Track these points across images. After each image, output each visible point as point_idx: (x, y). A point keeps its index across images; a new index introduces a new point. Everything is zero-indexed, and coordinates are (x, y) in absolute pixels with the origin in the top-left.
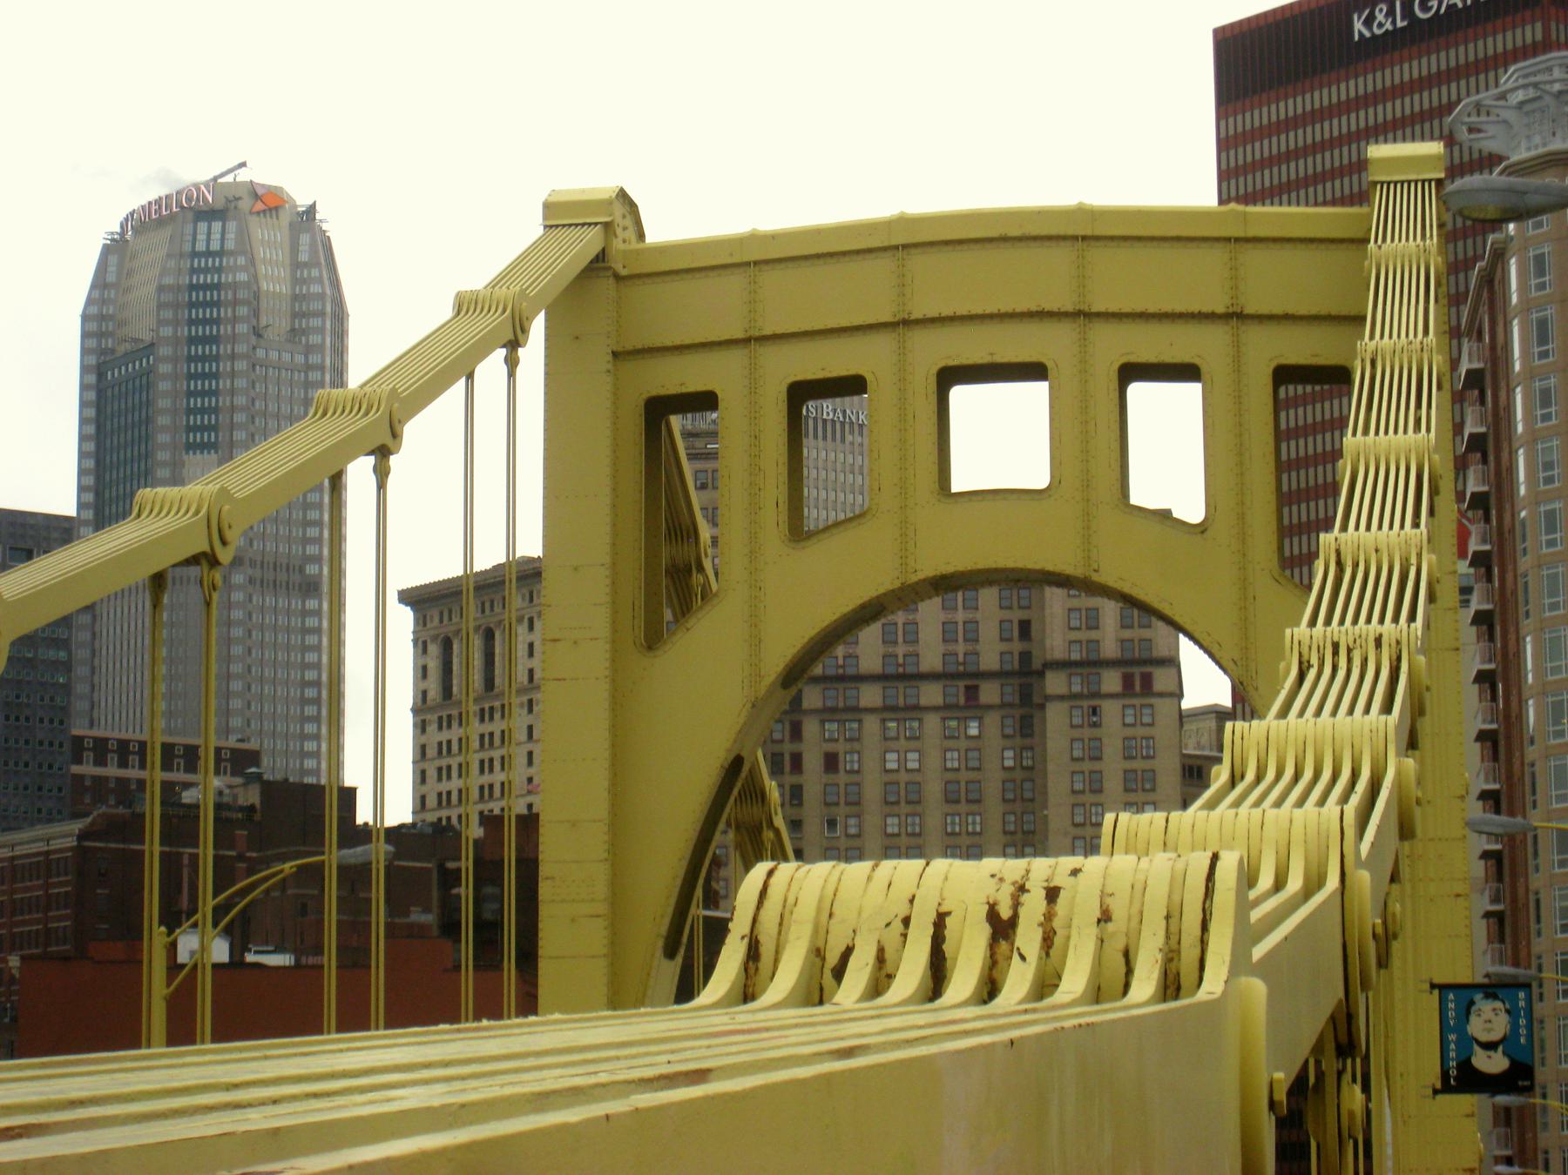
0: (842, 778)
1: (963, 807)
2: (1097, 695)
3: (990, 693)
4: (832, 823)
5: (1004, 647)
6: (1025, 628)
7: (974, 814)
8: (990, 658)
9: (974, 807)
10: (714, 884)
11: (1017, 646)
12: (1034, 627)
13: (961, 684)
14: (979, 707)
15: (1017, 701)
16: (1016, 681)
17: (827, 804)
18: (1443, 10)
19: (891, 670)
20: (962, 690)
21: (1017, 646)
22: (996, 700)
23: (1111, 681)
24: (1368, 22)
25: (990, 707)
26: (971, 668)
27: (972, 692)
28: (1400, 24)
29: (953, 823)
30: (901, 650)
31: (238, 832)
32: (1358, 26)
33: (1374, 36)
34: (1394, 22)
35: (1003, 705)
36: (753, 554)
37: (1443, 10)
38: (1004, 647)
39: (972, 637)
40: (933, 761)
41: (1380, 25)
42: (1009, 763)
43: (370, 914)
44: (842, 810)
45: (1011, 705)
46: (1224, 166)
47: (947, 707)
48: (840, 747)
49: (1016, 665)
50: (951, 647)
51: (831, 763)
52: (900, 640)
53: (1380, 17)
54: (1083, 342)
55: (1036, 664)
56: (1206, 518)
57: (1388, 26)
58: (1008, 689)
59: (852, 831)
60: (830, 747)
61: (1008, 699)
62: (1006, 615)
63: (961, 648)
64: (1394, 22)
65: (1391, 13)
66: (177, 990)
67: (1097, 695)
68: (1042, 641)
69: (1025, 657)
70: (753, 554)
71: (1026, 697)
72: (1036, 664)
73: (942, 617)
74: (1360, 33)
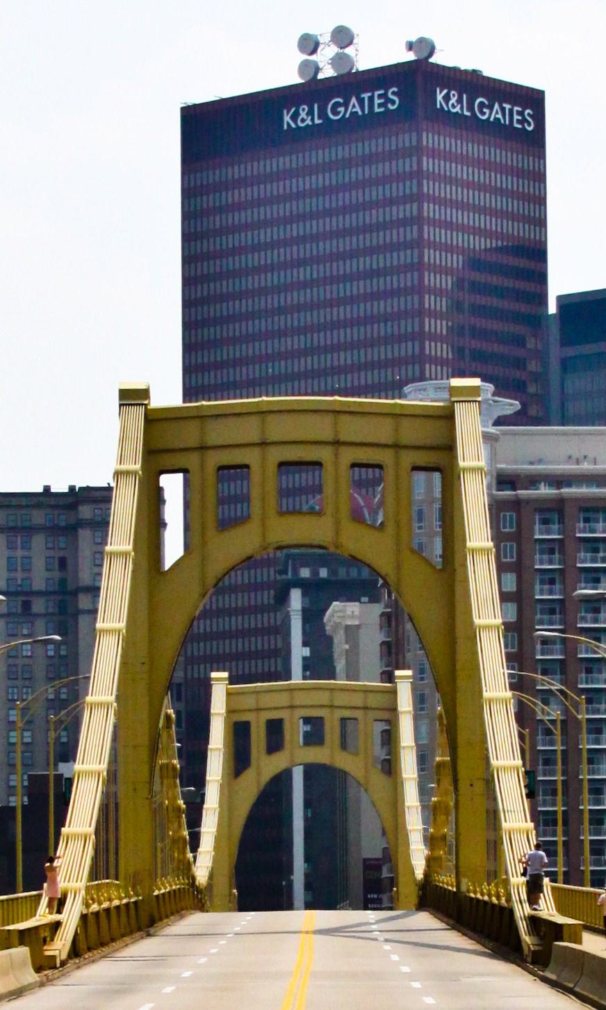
1: (19, 683)
3: (38, 606)
5: (47, 574)
6: (63, 563)
7: (27, 687)
8: (39, 584)
9: (27, 683)
10: (562, 587)
11: (57, 574)
12: (70, 562)
14: (30, 614)
15: (57, 610)
18: (347, 116)
20: (20, 603)
21: (57, 574)
22: (43, 611)
24: (295, 117)
25: (38, 615)
26: (26, 589)
27: (27, 606)
28: (317, 121)
29: (13, 694)
32: (287, 119)
34: (312, 120)
35: (9, 615)
36: (203, 535)
37: (347, 116)
38: (47, 574)
39: (27, 569)
41: (303, 120)
42: (51, 653)
43: (90, 672)
45: (52, 614)
49: (57, 588)
50: (12, 575)
52: (19, 569)
53: (303, 115)
54: (263, 422)
55: (70, 587)
57: (309, 122)
58: (51, 604)
61: (51, 610)
62: (51, 553)
63: (20, 575)
64: (312, 120)
65: (311, 113)
68: (76, 572)
69: (63, 582)
70: (203, 535)
72: (70, 587)
74: (288, 124)
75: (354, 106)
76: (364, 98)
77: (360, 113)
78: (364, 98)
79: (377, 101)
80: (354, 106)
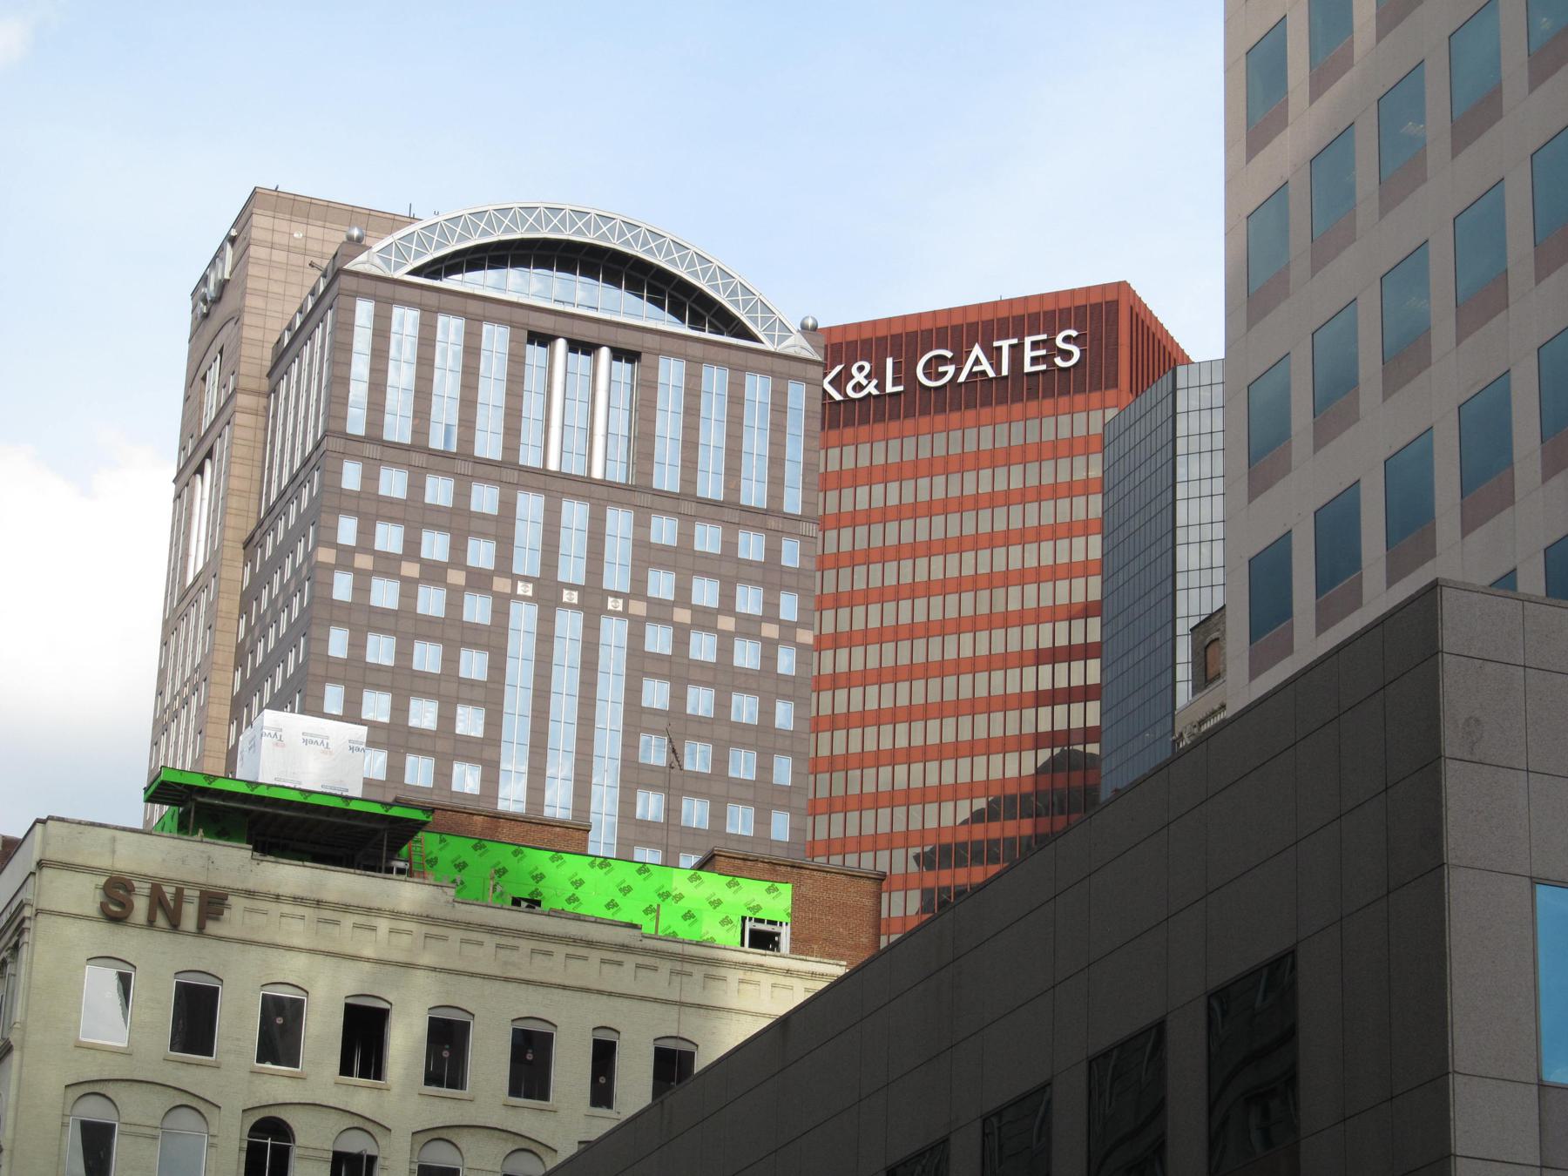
28: (890, 389)
41: (859, 387)
53: (859, 377)
57: (871, 389)
65: (878, 373)
75: (977, 362)
76: (1000, 349)
77: (991, 374)
78: (1000, 349)
79: (1028, 354)
80: (977, 362)
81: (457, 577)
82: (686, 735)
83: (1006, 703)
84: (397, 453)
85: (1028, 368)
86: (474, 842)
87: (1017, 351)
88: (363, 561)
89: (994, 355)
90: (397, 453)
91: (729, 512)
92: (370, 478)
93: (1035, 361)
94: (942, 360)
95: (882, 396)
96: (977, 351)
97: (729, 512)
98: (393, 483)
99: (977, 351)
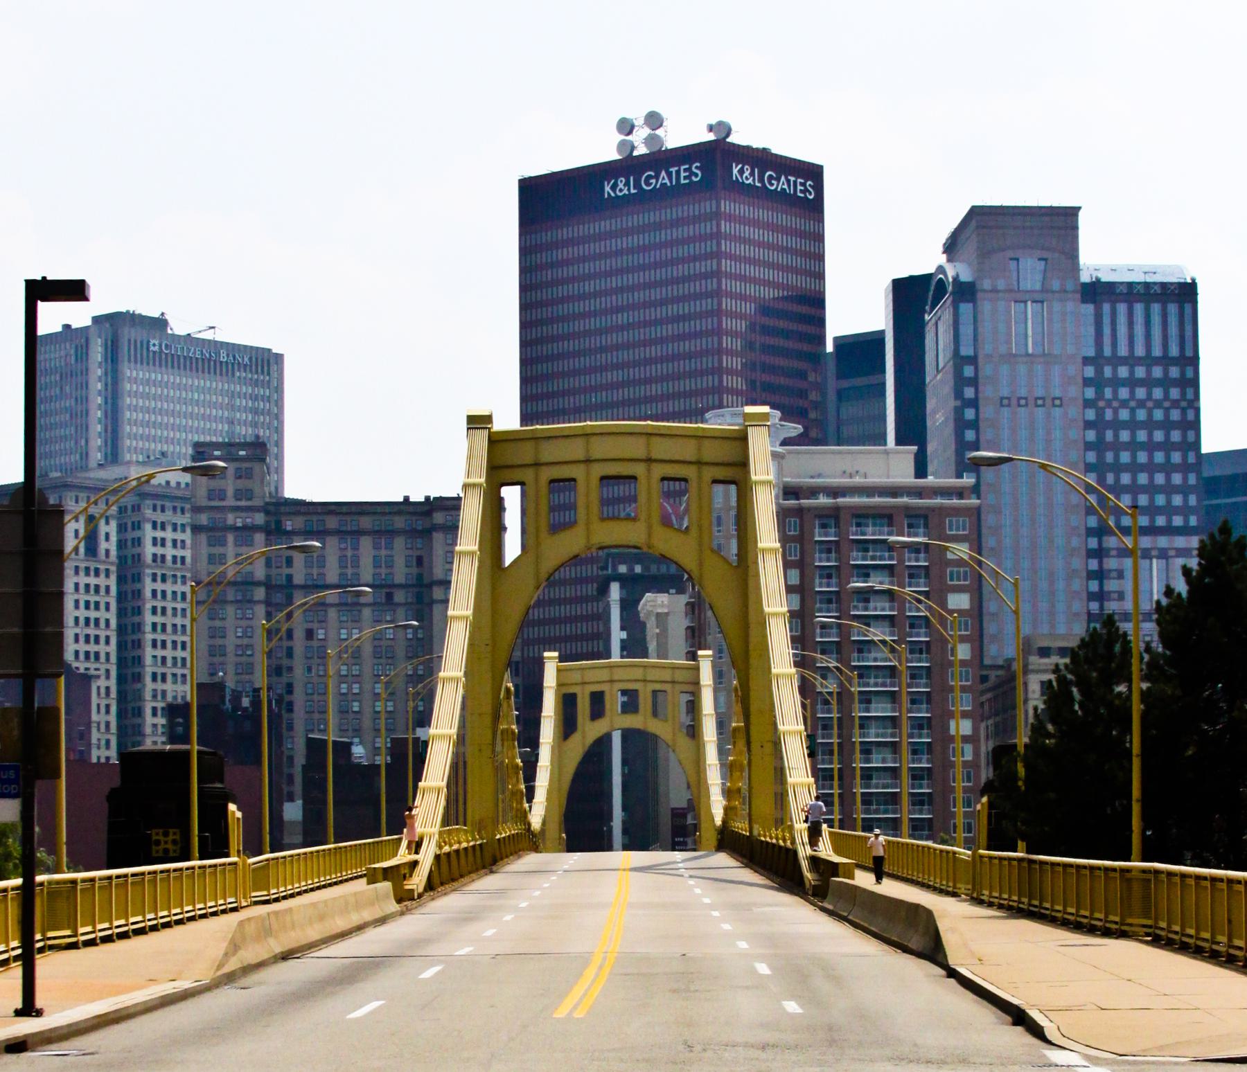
0: (315, 643)
1: (383, 661)
2: (250, 601)
3: (399, 596)
4: (310, 669)
6: (420, 561)
8: (399, 578)
11: (415, 570)
12: (425, 560)
13: (384, 590)
16: (416, 590)
17: (307, 658)
19: (310, 583)
21: (415, 570)
22: (403, 601)
23: (260, 593)
24: (614, 188)
25: (399, 604)
27: (389, 596)
28: (633, 191)
30: (315, 571)
31: (546, 654)
32: (607, 189)
33: (617, 197)
39: (390, 565)
40: (332, 634)
41: (621, 190)
44: (316, 661)
46: (1188, 308)
47: (340, 604)
48: (315, 626)
50: (378, 571)
51: (310, 634)
53: (621, 186)
56: (499, 492)
58: (410, 595)
59: (321, 673)
60: (310, 626)
63: (383, 571)
65: (627, 184)
66: (171, 752)
67: (250, 601)
71: (419, 598)
72: (426, 581)
73: (373, 552)
79: (683, 174)
81: (1115, 404)
82: (1129, 443)
83: (594, 314)
84: (1123, 361)
85: (683, 182)
86: (508, 418)
87: (678, 173)
88: (1115, 404)
89: (669, 175)
90: (1123, 361)
91: (1149, 361)
92: (1115, 371)
93: (685, 178)
94: (649, 177)
95: (630, 194)
96: (663, 173)
97: (1131, 361)
98: (1123, 372)
99: (663, 173)
